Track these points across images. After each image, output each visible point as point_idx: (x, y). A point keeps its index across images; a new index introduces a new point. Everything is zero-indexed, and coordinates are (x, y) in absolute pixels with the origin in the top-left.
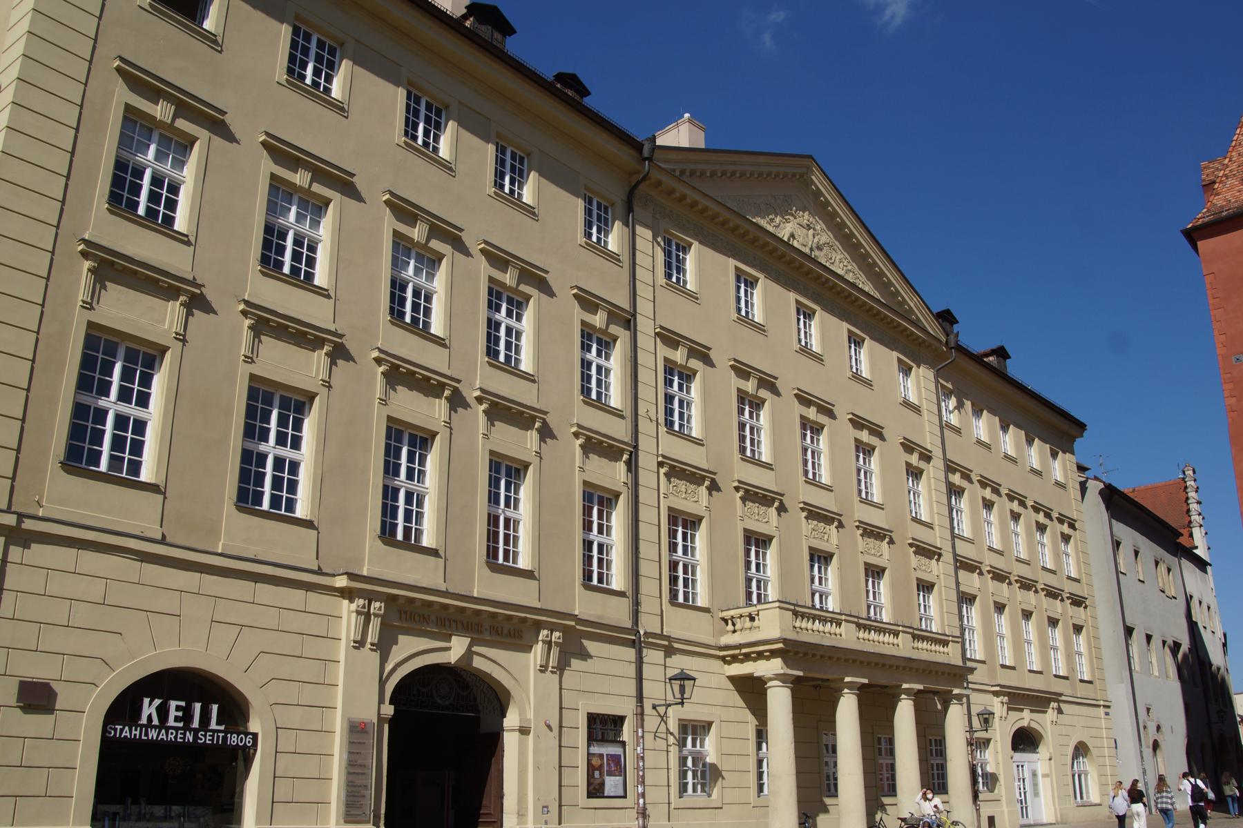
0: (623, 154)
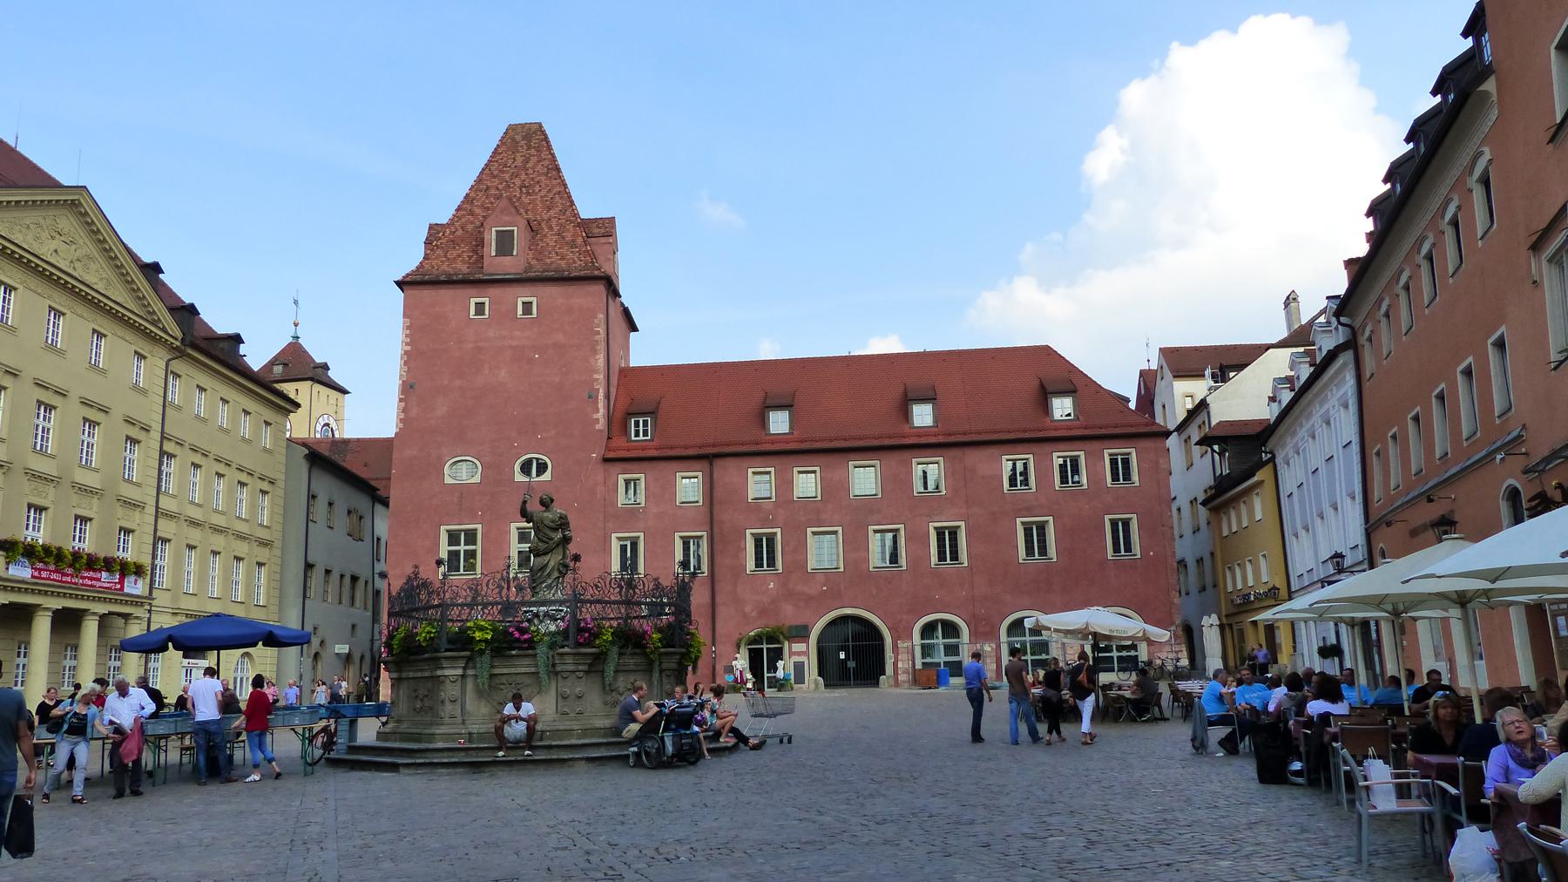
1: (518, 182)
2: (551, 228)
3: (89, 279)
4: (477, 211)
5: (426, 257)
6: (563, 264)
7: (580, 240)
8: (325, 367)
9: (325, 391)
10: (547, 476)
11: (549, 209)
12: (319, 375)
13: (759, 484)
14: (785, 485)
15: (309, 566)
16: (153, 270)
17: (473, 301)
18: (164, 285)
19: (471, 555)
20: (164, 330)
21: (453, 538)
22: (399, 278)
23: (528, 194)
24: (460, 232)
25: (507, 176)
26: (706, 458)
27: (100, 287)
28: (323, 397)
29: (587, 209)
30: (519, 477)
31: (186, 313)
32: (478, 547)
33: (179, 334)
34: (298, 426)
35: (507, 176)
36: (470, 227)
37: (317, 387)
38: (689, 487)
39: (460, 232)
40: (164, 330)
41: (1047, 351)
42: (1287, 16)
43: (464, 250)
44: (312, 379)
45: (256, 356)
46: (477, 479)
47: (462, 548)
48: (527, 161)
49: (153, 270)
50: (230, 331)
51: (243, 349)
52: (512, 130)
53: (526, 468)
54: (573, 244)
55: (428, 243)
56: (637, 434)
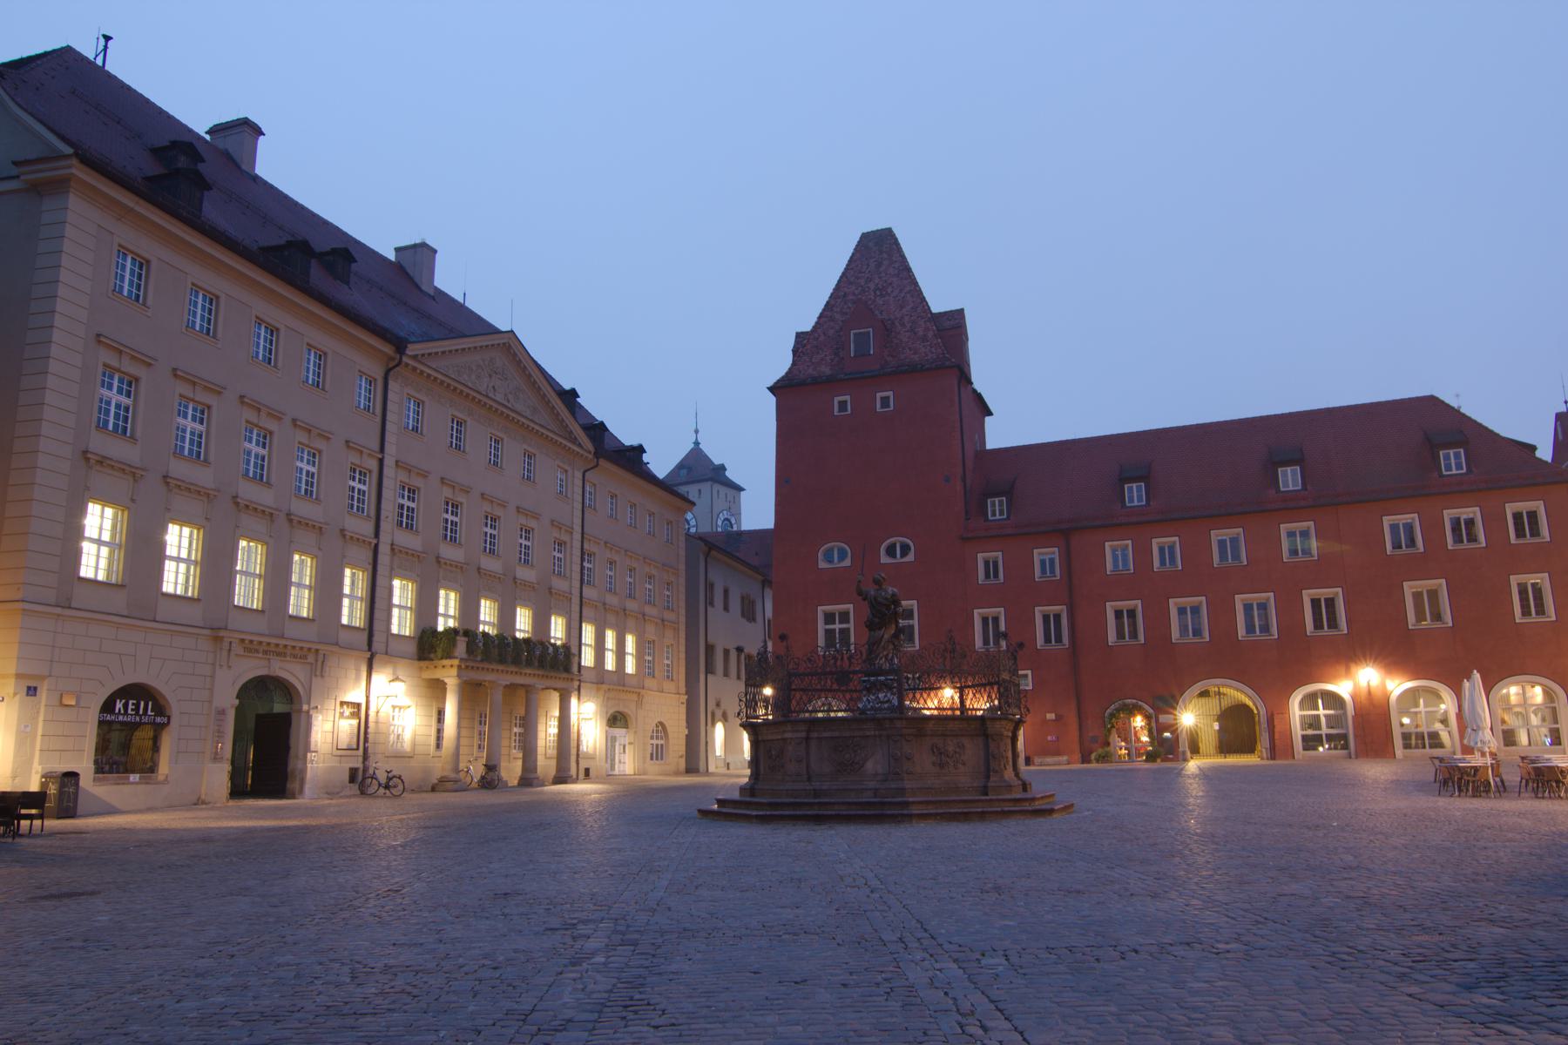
0: (388, 349)
1: (872, 286)
2: (903, 325)
3: (519, 407)
4: (837, 316)
5: (794, 363)
6: (916, 357)
7: (930, 334)
8: (722, 468)
9: (723, 490)
10: (911, 557)
11: (902, 307)
12: (717, 475)
13: (1116, 553)
14: (1143, 553)
15: (710, 649)
16: (573, 394)
17: (837, 400)
18: (581, 407)
19: (844, 632)
20: (580, 445)
21: (829, 618)
22: (770, 384)
23: (882, 296)
24: (822, 338)
25: (862, 282)
26: (1063, 533)
27: (528, 413)
28: (722, 495)
29: (938, 303)
30: (885, 559)
31: (597, 430)
32: (851, 626)
33: (592, 449)
34: (695, 521)
35: (862, 282)
36: (831, 332)
37: (717, 487)
38: (1045, 555)
39: (822, 338)
40: (580, 445)
41: (1432, 400)
42: (808, 328)
43: (175, 554)
44: (711, 479)
45: (661, 463)
46: (847, 563)
47: (837, 626)
48: (879, 265)
49: (573, 394)
50: (635, 443)
51: (645, 458)
52: (865, 238)
53: (891, 551)
54: (924, 339)
55: (795, 351)
56: (994, 514)
